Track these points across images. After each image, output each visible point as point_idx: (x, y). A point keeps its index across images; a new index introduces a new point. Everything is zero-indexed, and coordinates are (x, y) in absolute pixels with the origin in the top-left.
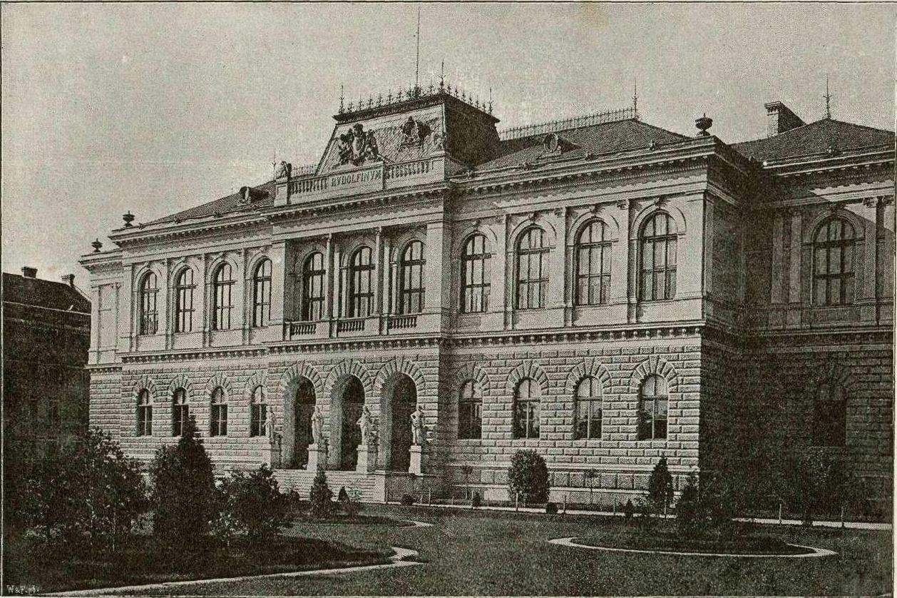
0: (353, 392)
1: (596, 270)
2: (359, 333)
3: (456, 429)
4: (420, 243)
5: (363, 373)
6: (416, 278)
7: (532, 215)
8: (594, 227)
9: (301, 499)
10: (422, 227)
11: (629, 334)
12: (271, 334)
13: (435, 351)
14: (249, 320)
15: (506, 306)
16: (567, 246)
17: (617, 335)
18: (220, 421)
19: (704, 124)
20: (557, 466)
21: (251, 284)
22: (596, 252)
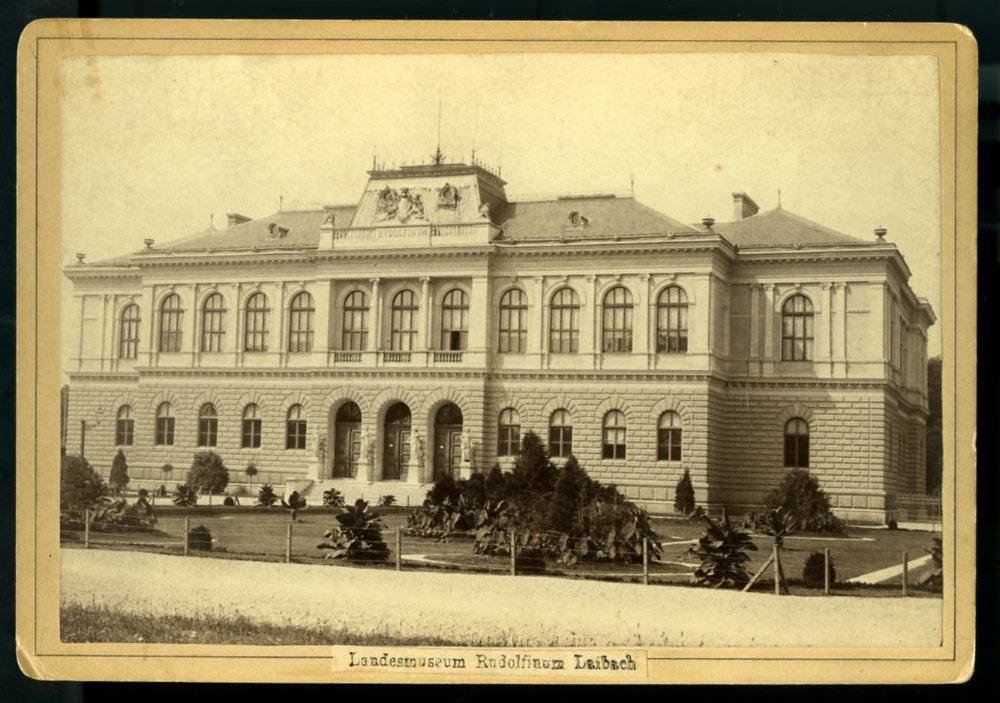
0: (396, 414)
1: (566, 326)
2: (407, 365)
3: (495, 448)
4: (409, 293)
5: (305, 398)
6: (260, 323)
7: (565, 278)
8: (796, 302)
9: (626, 500)
10: (468, 280)
11: (542, 377)
12: (317, 360)
13: (480, 383)
14: (285, 343)
15: (281, 349)
16: (595, 306)
17: (532, 376)
18: (297, 435)
19: (881, 233)
20: (697, 472)
21: (286, 314)
22: (515, 314)
